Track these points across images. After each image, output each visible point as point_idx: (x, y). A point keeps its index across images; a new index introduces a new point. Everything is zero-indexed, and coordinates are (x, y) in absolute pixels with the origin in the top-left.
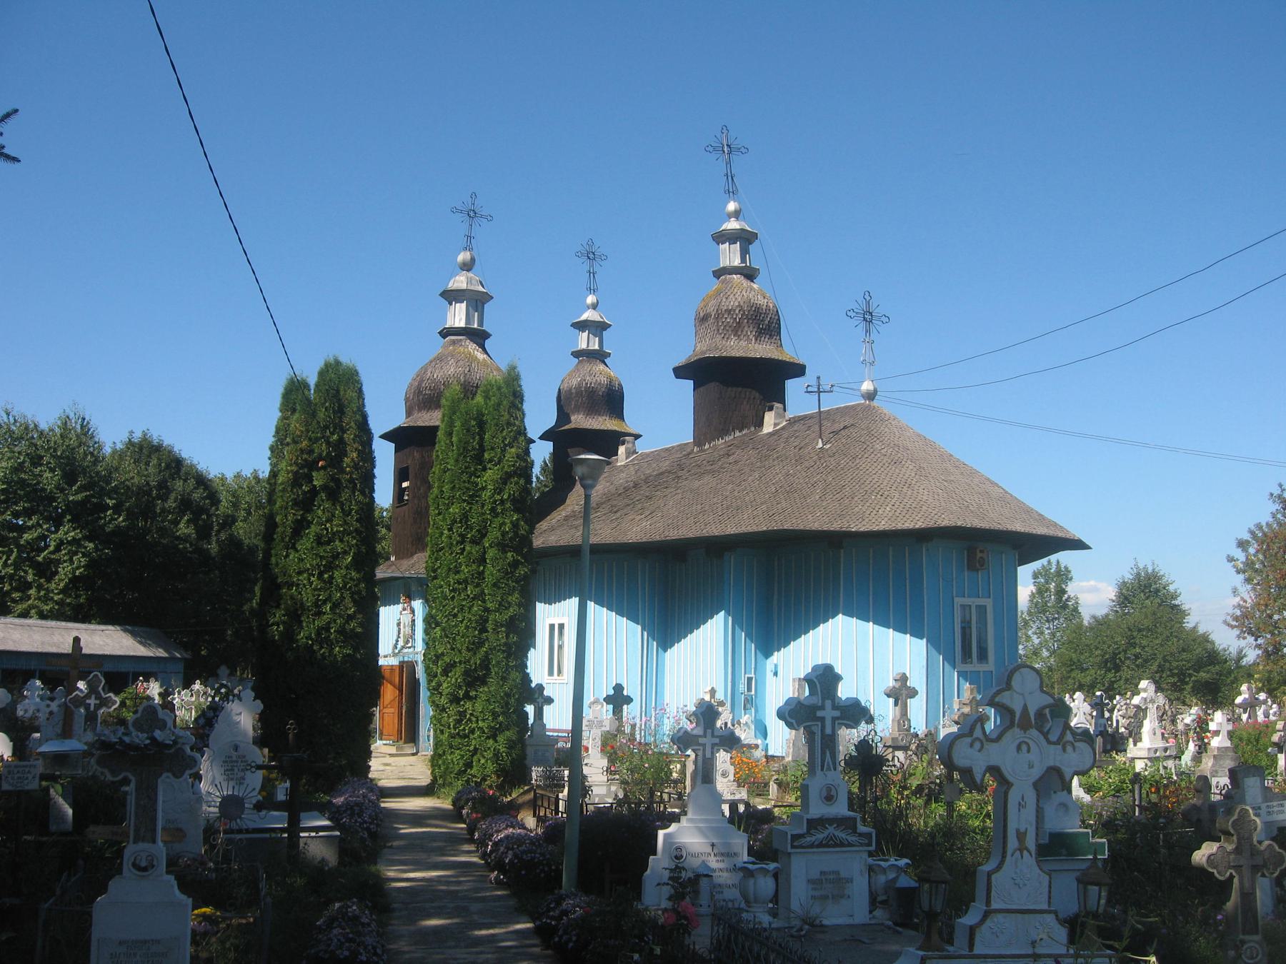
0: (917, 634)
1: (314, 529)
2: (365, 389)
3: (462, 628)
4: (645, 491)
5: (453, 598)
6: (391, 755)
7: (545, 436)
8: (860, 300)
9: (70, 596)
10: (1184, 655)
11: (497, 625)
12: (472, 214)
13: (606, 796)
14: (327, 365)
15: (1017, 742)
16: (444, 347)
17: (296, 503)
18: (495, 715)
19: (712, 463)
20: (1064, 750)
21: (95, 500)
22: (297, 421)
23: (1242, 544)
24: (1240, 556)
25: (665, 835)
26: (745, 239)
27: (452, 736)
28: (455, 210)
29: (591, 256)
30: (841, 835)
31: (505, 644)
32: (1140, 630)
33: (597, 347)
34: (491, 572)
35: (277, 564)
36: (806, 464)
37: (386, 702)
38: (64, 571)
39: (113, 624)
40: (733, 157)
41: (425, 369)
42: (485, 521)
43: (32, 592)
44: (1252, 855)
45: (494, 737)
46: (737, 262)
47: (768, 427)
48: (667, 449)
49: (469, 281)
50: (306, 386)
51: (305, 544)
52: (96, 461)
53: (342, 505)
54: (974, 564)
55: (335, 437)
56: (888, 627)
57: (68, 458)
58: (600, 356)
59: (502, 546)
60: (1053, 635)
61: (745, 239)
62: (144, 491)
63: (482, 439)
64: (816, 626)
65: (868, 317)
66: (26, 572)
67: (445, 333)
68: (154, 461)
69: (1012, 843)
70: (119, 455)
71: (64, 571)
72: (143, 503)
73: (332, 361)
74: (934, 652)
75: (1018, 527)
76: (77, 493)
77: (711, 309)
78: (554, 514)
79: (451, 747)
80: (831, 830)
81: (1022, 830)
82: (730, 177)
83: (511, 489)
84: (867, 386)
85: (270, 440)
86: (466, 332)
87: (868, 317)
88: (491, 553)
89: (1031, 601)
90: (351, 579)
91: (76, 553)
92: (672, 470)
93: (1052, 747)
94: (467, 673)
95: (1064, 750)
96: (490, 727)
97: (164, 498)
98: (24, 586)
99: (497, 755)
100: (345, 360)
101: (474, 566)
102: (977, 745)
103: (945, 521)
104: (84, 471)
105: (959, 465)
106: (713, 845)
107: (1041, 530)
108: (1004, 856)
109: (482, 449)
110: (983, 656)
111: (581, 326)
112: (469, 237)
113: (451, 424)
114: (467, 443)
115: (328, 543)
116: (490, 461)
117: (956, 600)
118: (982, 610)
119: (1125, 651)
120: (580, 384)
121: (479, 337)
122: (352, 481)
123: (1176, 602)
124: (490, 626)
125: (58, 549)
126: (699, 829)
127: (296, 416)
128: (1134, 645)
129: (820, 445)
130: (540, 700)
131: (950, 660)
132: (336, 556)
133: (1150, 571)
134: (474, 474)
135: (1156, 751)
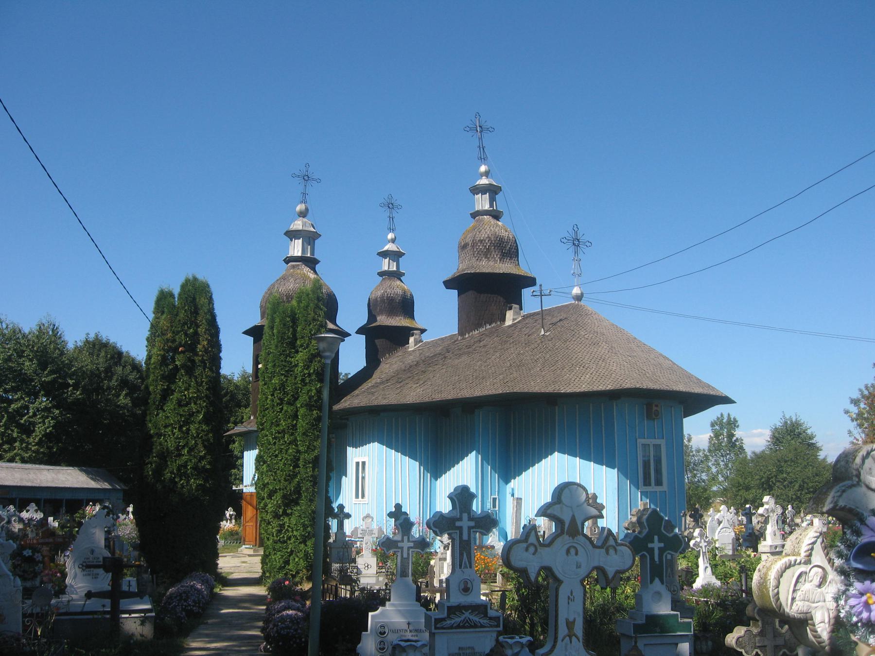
0: (611, 465)
1: (176, 395)
2: (214, 297)
3: (281, 465)
4: (422, 367)
5: (275, 443)
6: (250, 556)
7: (360, 331)
8: (571, 230)
9: (43, 447)
10: (817, 478)
11: (306, 462)
12: (306, 178)
13: (375, 584)
14: (187, 280)
15: (566, 547)
16: (287, 270)
17: (164, 377)
18: (305, 526)
19: (469, 347)
20: (607, 553)
21: (60, 381)
22: (165, 320)
23: (855, 402)
24: (854, 410)
25: (372, 616)
26: (493, 191)
27: (275, 542)
28: (294, 176)
29: (390, 206)
30: (475, 618)
31: (312, 476)
32: (786, 461)
33: (395, 269)
34: (302, 424)
35: (150, 421)
36: (533, 346)
37: (248, 518)
38: (39, 430)
39: (73, 466)
40: (484, 134)
41: (273, 285)
42: (297, 388)
43: (17, 444)
44: (775, 636)
45: (304, 542)
46: (487, 207)
47: (509, 322)
48: (442, 339)
49: (304, 224)
50: (171, 295)
51: (169, 406)
52: (62, 353)
53: (196, 378)
54: (651, 414)
55: (191, 330)
56: (590, 461)
57: (42, 352)
58: (397, 275)
59: (310, 406)
60: (726, 465)
61: (493, 191)
62: (94, 375)
63: (295, 331)
64: (540, 460)
65: (576, 243)
66: (13, 431)
67: (288, 260)
68: (103, 354)
69: (563, 630)
70: (79, 350)
71: (39, 430)
72: (94, 382)
73: (191, 277)
74: (622, 477)
75: (681, 388)
76: (47, 376)
77: (469, 240)
78: (365, 384)
79: (274, 550)
80: (467, 614)
81: (571, 619)
82: (482, 148)
83: (315, 366)
84: (576, 291)
85: (147, 334)
86: (302, 259)
87: (576, 243)
88: (302, 411)
89: (710, 442)
90: (203, 431)
91: (47, 417)
92: (446, 351)
93: (598, 550)
94: (284, 497)
95: (607, 553)
96: (301, 535)
97: (110, 379)
98: (11, 441)
99: (306, 555)
100: (200, 277)
101: (289, 421)
102: (532, 549)
103: (628, 385)
104: (53, 361)
105: (642, 346)
106: (409, 624)
107: (697, 390)
108: (555, 641)
109: (295, 338)
110: (659, 483)
111: (384, 254)
112: (304, 194)
113: (273, 320)
114: (284, 333)
115: (186, 405)
116: (302, 346)
117: (639, 440)
118: (657, 447)
119: (776, 476)
120: (383, 295)
121: (311, 262)
122: (203, 361)
123: (813, 441)
124: (301, 463)
125: (35, 415)
126: (399, 611)
127: (164, 317)
128: (782, 472)
129: (543, 333)
130: (341, 516)
131: (635, 483)
132: (192, 414)
133: (794, 420)
134: (289, 355)
135: (776, 547)
